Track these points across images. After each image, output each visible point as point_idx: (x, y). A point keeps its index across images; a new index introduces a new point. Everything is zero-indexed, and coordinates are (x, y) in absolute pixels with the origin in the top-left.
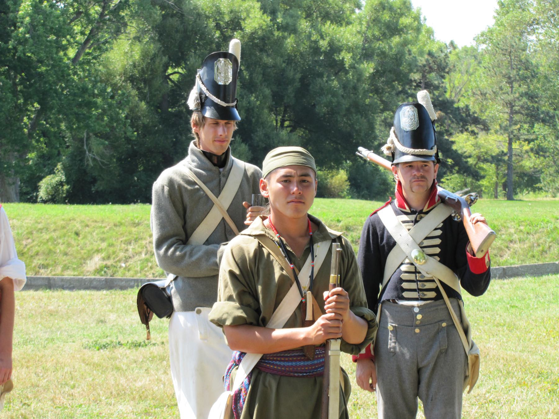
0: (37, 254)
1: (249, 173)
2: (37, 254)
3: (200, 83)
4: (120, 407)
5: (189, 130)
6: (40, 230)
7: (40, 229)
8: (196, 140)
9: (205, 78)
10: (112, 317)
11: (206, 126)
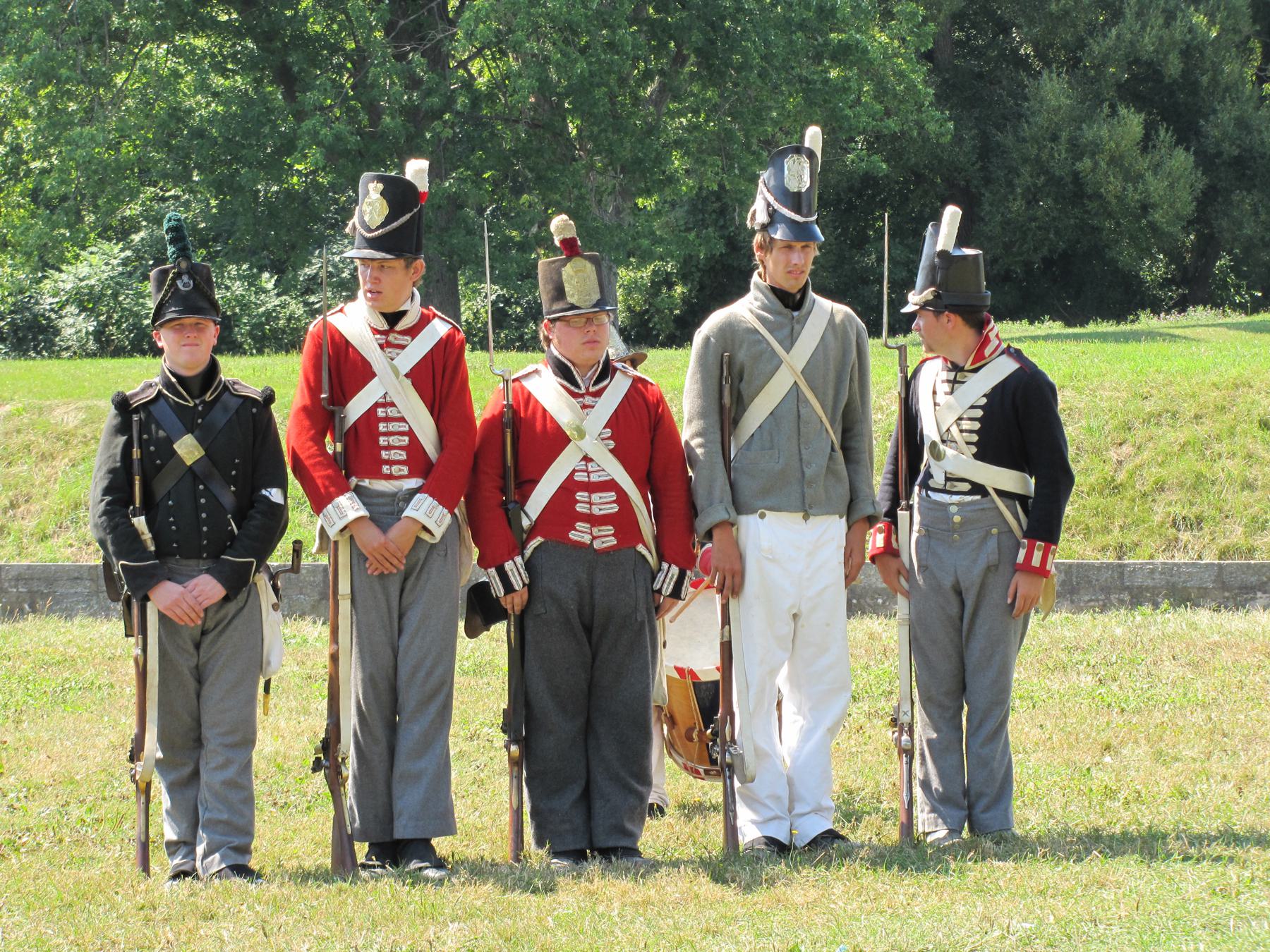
0: (1160, 487)
1: (838, 319)
2: (1160, 487)
3: (765, 190)
5: (751, 256)
6: (1154, 418)
7: (1151, 415)
8: (761, 269)
9: (772, 183)
11: (774, 252)
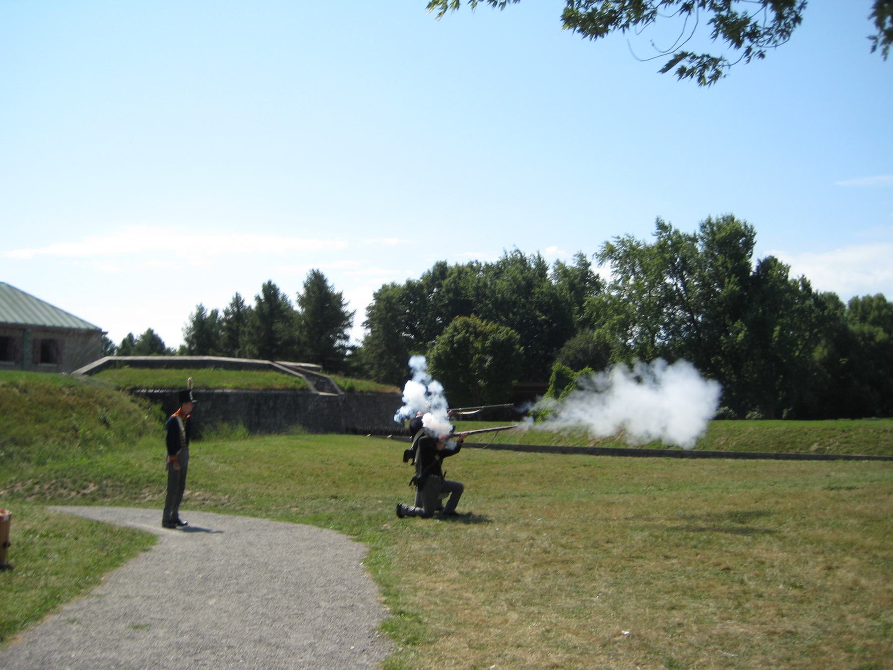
4: (851, 521)
6: (789, 432)
10: (833, 474)
